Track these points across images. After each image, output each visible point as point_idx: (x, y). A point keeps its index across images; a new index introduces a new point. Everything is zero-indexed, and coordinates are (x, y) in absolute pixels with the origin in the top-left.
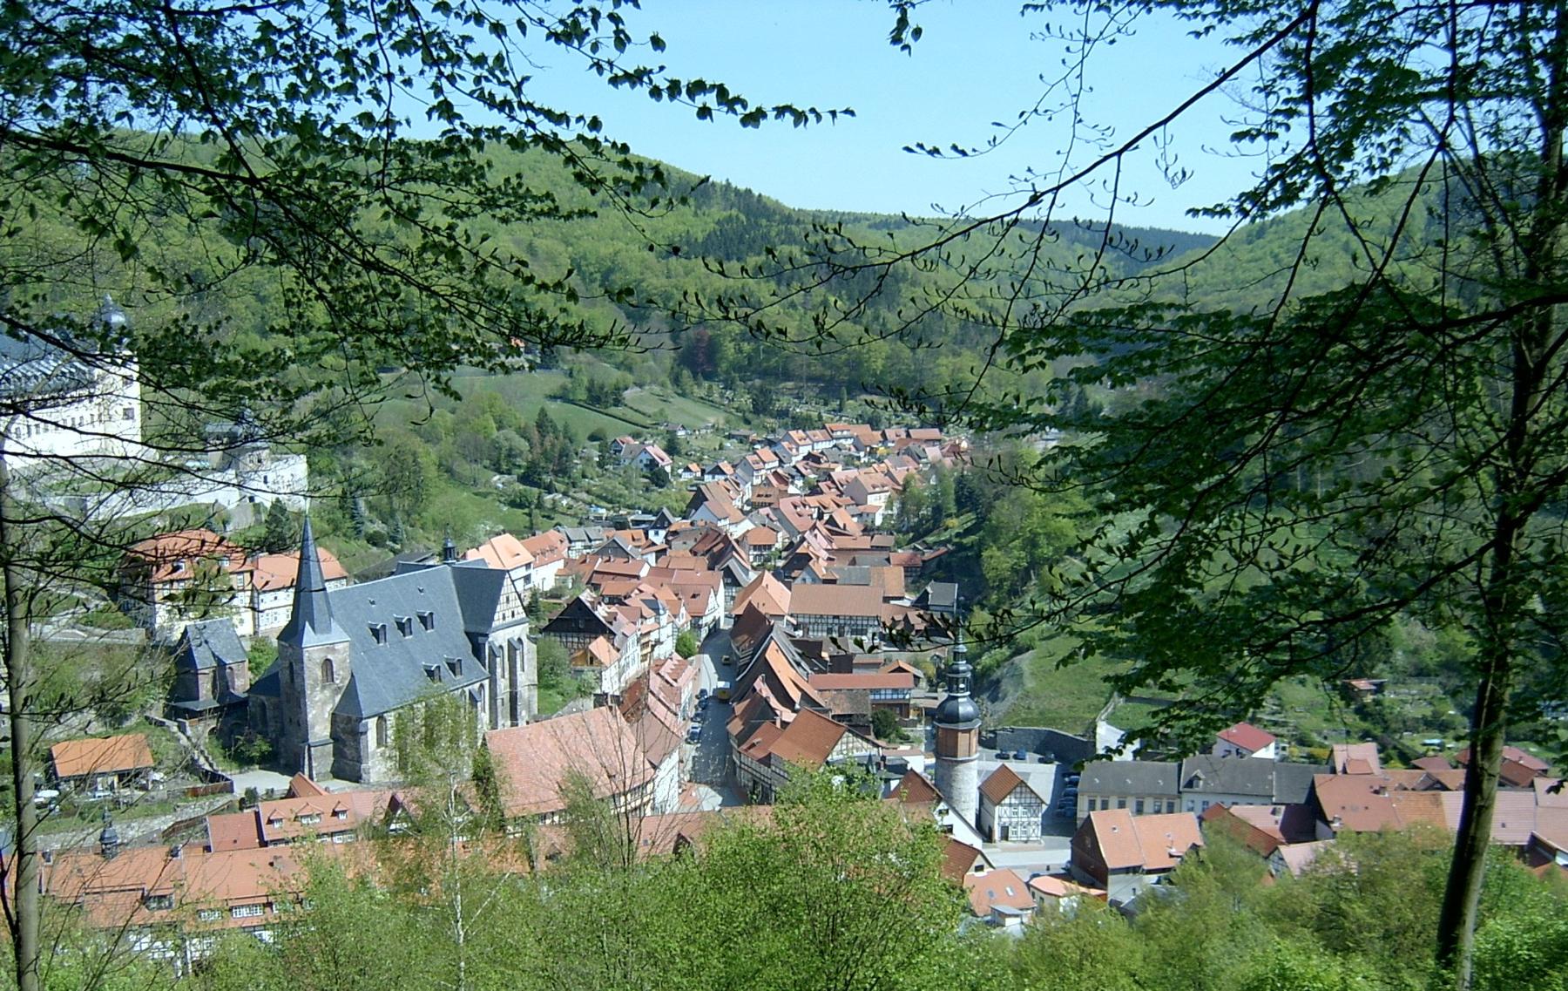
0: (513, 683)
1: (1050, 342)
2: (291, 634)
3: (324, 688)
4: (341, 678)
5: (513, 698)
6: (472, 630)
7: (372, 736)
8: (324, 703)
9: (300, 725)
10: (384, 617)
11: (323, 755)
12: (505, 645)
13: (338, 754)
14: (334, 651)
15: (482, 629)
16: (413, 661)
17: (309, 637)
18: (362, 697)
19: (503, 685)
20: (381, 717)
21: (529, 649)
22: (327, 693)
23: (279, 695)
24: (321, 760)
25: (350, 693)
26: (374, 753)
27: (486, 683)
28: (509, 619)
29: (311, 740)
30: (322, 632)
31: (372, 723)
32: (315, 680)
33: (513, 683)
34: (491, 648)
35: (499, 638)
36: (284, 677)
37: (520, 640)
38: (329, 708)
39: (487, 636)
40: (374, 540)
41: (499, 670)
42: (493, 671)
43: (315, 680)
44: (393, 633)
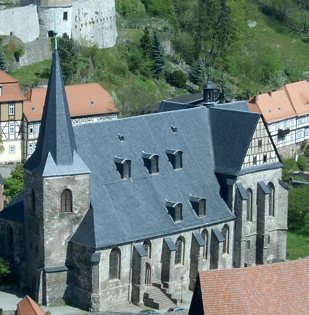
0: (260, 226)
1: (161, 61)
2: (33, 165)
3: (62, 216)
4: (80, 208)
5: (260, 242)
6: (223, 170)
7: (103, 268)
8: (62, 231)
9: (37, 251)
10: (134, 154)
11: (57, 282)
12: (254, 188)
13: (72, 281)
14: (73, 181)
15: (230, 171)
16: (156, 198)
17: (50, 167)
18: (98, 228)
19: (249, 228)
20: (116, 250)
21: (281, 195)
22: (65, 222)
23: (23, 222)
24: (56, 285)
25: (87, 224)
26: (105, 285)
27: (231, 224)
28: (260, 163)
29: (47, 266)
30: (64, 163)
31: (105, 255)
32: (54, 209)
33: (260, 226)
34: (238, 190)
35: (247, 181)
36: (28, 204)
37: (271, 185)
38: (66, 237)
39: (234, 178)
40: (175, 80)
41: (244, 213)
42: (238, 213)
43: (54, 209)
44: (138, 169)
